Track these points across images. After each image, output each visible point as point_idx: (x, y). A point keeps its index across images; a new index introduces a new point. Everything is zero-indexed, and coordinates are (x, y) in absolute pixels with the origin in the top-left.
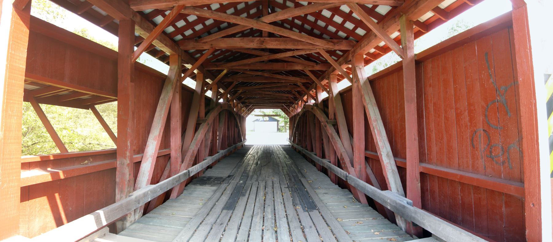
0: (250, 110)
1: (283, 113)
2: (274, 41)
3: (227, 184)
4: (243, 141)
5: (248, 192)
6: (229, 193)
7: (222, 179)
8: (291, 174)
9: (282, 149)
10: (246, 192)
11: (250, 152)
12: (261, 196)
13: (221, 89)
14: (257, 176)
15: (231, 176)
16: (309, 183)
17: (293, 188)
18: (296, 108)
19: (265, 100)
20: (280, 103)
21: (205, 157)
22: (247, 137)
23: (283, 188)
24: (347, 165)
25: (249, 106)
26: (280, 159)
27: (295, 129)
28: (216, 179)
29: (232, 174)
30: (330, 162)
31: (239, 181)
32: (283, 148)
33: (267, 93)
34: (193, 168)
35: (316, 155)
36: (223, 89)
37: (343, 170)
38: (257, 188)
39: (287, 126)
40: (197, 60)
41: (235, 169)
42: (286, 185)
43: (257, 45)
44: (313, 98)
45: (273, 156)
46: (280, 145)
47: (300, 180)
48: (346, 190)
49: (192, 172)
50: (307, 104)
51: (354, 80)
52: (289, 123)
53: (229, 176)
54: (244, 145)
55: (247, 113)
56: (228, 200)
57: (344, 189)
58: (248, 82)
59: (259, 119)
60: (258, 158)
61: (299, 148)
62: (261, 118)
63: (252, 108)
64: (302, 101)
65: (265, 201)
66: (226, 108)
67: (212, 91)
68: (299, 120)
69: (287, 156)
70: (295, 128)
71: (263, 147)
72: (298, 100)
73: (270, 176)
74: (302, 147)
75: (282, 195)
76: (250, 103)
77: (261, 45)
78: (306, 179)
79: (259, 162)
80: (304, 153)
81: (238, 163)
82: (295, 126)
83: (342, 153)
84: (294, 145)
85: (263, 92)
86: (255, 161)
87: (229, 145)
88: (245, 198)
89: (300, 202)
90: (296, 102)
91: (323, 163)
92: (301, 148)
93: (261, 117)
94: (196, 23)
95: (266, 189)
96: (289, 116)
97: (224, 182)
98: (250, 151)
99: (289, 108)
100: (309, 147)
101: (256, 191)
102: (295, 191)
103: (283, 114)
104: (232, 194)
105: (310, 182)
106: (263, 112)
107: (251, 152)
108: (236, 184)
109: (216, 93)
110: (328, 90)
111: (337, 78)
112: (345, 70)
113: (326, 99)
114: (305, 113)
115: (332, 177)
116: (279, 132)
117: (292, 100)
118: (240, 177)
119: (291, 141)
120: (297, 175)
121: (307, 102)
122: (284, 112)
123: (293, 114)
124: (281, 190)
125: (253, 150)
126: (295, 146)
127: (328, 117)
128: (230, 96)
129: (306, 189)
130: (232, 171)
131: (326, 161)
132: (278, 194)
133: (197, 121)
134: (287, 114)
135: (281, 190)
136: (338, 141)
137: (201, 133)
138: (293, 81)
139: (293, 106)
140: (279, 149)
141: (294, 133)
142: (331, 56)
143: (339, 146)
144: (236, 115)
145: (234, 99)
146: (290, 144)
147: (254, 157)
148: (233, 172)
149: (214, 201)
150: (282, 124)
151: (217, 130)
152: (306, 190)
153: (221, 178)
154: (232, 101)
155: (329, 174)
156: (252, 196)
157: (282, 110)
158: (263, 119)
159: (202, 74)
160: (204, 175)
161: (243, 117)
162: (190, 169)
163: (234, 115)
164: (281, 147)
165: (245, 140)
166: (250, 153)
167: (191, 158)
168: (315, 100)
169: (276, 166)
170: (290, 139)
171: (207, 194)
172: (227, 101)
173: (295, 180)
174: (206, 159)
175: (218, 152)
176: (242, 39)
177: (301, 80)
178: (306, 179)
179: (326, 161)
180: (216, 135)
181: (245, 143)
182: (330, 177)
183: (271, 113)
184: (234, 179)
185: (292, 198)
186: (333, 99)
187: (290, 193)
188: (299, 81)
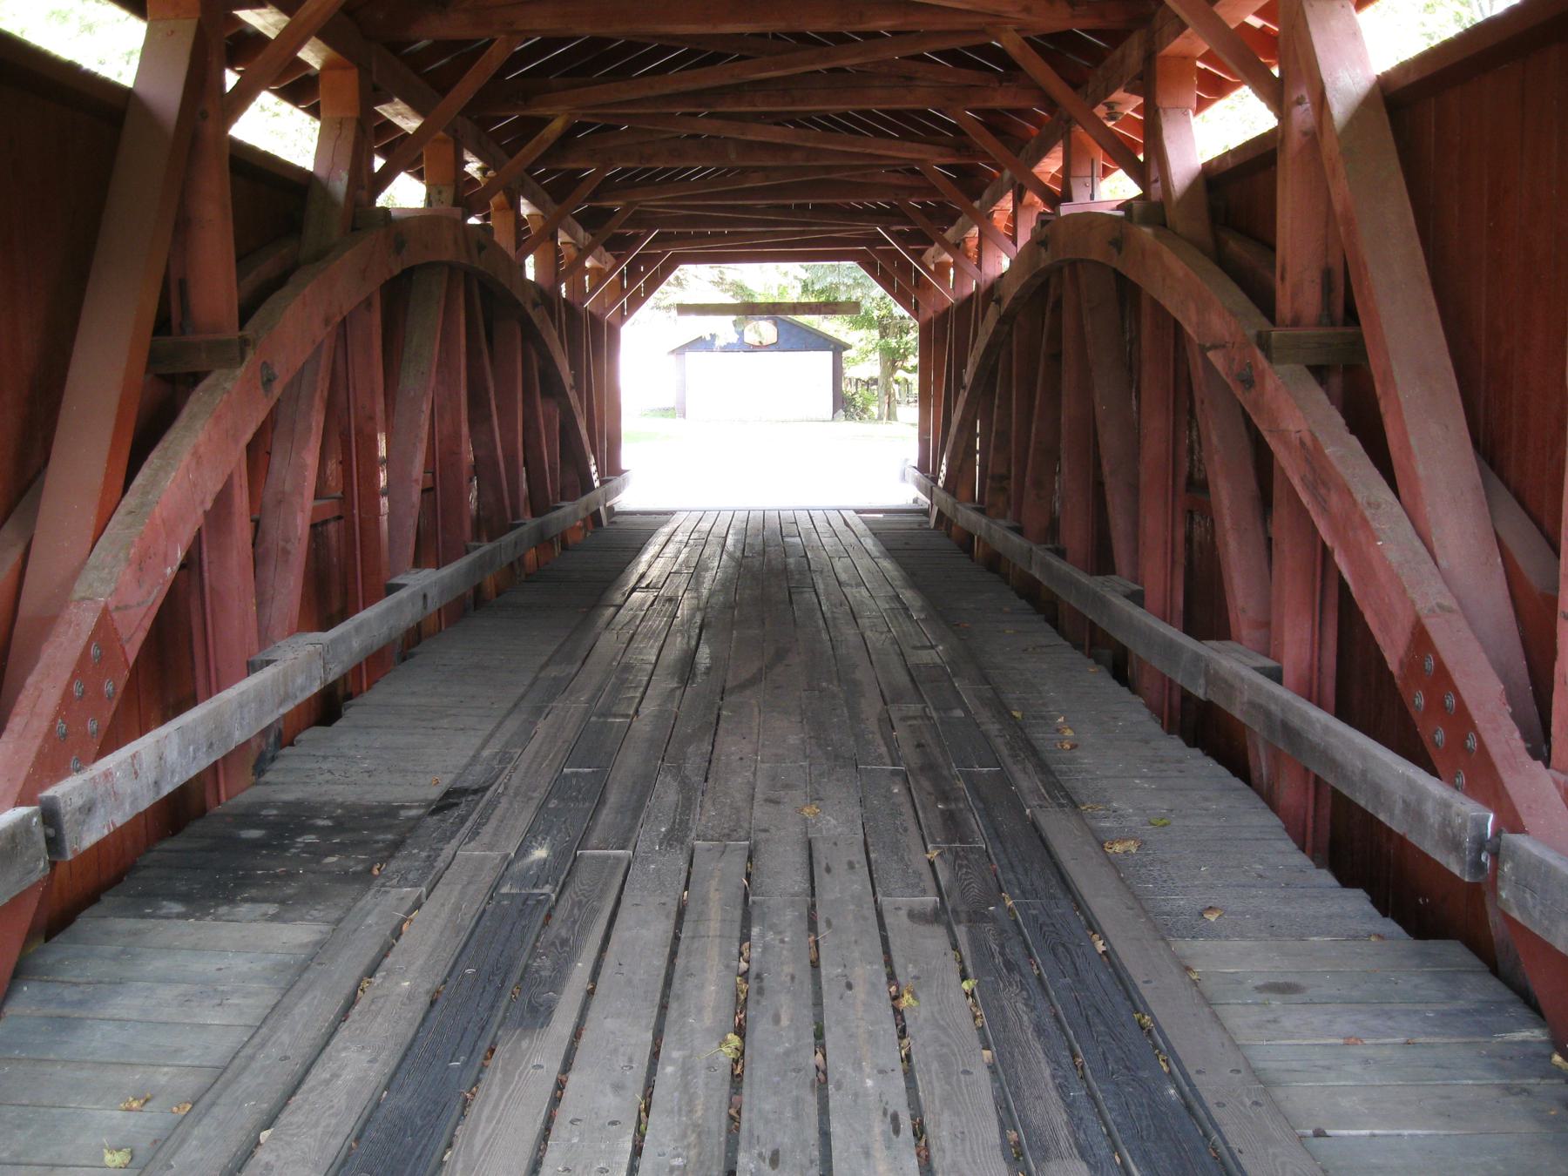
0: (647, 271)
1: (878, 291)
3: (415, 885)
4: (602, 483)
5: (581, 969)
6: (411, 996)
7: (388, 828)
8: (955, 770)
9: (869, 543)
10: (558, 980)
11: (642, 568)
12: (708, 1019)
13: (400, 106)
14: (685, 785)
15: (463, 792)
16: (1113, 863)
17: (988, 926)
18: (973, 253)
20: (853, 214)
21: (555, 501)
22: (628, 456)
23: (897, 922)
24: (1488, 738)
25: (636, 240)
26: (863, 622)
27: (967, 403)
28: (339, 826)
29: (470, 781)
30: (1276, 676)
31: (523, 851)
32: (877, 532)
33: (757, 134)
34: (107, 775)
35: (1137, 598)
36: (418, 108)
37: (1433, 772)
38: (672, 922)
39: (897, 382)
40: (443, 91)
41: (513, 724)
42: (924, 892)
44: (1121, 154)
45: (809, 596)
46: (858, 512)
47: (1035, 827)
48: (1454, 952)
49: (88, 809)
50: (1065, 210)
51: (1154, 174)
52: (913, 361)
53: (449, 800)
54: (610, 510)
55: (623, 291)
56: (387, 1087)
57: (1434, 946)
59: (713, 336)
60: (698, 619)
61: (995, 532)
62: (723, 326)
64: (1018, 200)
65: (736, 1080)
66: (447, 256)
67: (314, 111)
68: (995, 333)
69: (908, 595)
70: (963, 395)
71: (742, 515)
72: (986, 195)
73: (787, 786)
74: (1019, 531)
75: (898, 1012)
76: (642, 220)
78: (1080, 815)
79: (704, 656)
80: (1036, 573)
81: (543, 667)
82: (968, 378)
83: (1431, 625)
84: (956, 509)
85: (731, 131)
86: (678, 644)
87: (490, 524)
88: (544, 1052)
89: (1070, 1106)
90: (977, 204)
91: (1214, 679)
92: (1015, 538)
93: (730, 319)
95: (755, 931)
96: (915, 311)
97: (394, 865)
98: (646, 558)
99: (918, 255)
100: (1075, 534)
101: (660, 963)
102: (1010, 966)
103: (873, 294)
104: (433, 1003)
105: (1118, 848)
106: (739, 288)
107: (653, 563)
108: (487, 878)
109: (349, 134)
110: (1276, 71)
112: (1256, 22)
113: (1230, 163)
114: (1044, 286)
115: (1289, 791)
116: (849, 417)
118: (538, 795)
119: (935, 480)
120: (1004, 780)
121: (1067, 197)
122: (885, 281)
123: (951, 290)
124: (885, 942)
125: (671, 550)
126: (967, 517)
127: (1271, 317)
128: (483, 171)
129: (1104, 937)
130: (483, 747)
131: (1236, 666)
132: (860, 992)
133: (154, 358)
134: (902, 297)
135: (885, 942)
136: (1378, 506)
137: (186, 457)
138: (959, 23)
139: (950, 234)
140: (849, 538)
141: (953, 430)
143: (1393, 556)
144: (535, 305)
146: (925, 501)
147: (669, 607)
148: (486, 753)
149: (252, 1110)
150: (864, 366)
151: (372, 418)
152: (1100, 947)
153: (390, 811)
155: (1262, 764)
156: (610, 1024)
157: (870, 266)
158: (741, 334)
159: (356, 71)
160: (250, 795)
161: (596, 322)
162: (67, 790)
163: (518, 305)
164: (865, 521)
165: (616, 482)
166: (642, 576)
167: (77, 689)
168: (1139, 173)
169: (834, 688)
170: (922, 467)
171: (214, 1018)
172: (457, 202)
173: (996, 834)
174: (268, 663)
175: (392, 589)
178: (1080, 815)
179: (1236, 666)
180: (370, 463)
181: (616, 499)
182: (1269, 799)
183: (794, 296)
184: (488, 830)
185: (987, 1054)
186: (1330, 146)
187: (966, 986)
188: (935, 161)
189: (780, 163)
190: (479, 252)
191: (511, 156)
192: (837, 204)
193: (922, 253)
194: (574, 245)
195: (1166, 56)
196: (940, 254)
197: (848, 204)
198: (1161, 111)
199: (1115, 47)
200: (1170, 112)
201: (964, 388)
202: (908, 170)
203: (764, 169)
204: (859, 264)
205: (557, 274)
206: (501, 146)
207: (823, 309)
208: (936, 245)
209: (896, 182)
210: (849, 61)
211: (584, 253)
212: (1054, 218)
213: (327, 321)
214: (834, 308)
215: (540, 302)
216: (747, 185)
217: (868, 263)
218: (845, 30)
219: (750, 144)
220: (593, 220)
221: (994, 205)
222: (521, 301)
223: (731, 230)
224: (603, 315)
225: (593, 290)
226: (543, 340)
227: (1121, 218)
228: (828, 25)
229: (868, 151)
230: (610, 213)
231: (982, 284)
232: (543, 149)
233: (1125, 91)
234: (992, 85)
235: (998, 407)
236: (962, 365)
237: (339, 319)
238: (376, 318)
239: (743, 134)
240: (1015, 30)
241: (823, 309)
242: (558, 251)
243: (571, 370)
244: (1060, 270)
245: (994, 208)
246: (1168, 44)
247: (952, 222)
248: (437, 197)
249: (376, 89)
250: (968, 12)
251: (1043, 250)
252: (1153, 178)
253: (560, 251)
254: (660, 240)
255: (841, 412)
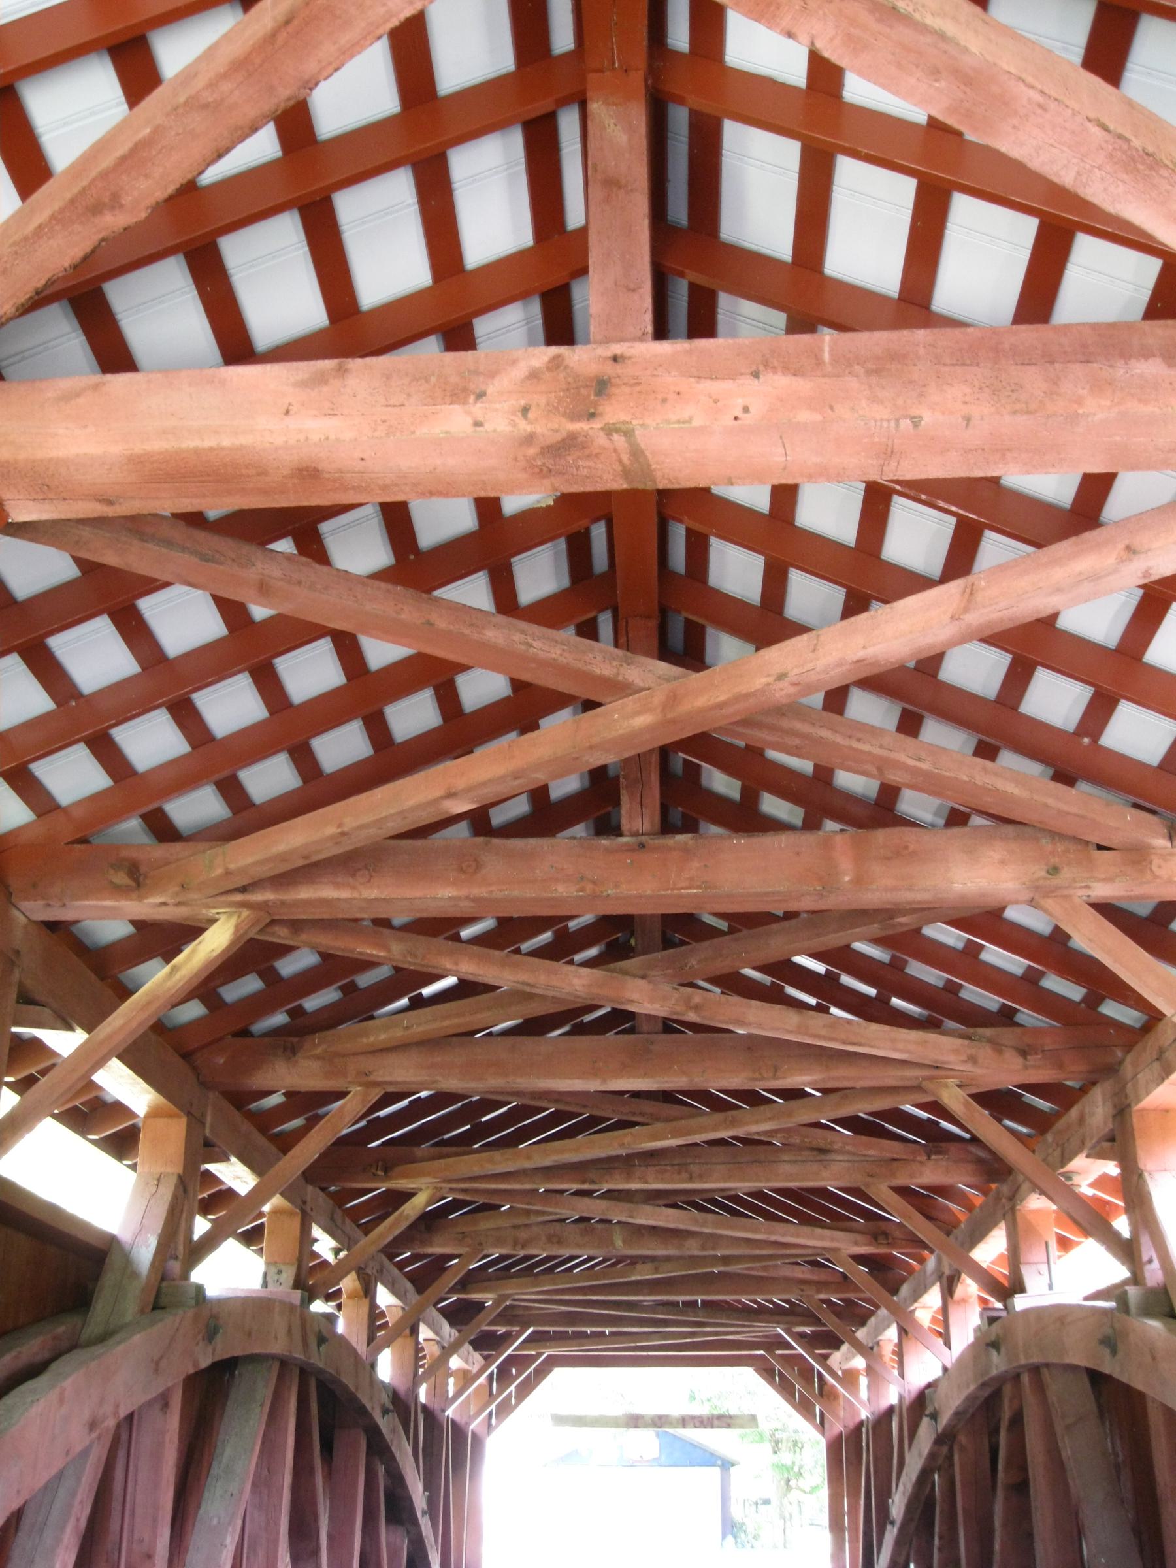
0: (519, 1374)
2: (733, 376)
19: (636, 1287)
20: (760, 1313)
25: (507, 1338)
27: (898, 1543)
40: (285, 1143)
43: (524, 427)
50: (1020, 1303)
51: (1147, 1251)
58: (555, 1257)
63: (531, 1359)
64: (949, 1291)
66: (277, 1347)
67: (260, 1252)
72: (905, 1290)
76: (512, 1315)
77: (574, 417)
82: (897, 1506)
85: (618, 1213)
94: (310, 981)
109: (167, 1192)
111: (1057, 1234)
117: (831, 1323)
121: (1018, 1286)
134: (804, 1408)
139: (861, 1334)
142: (999, 1121)
144: (385, 1412)
145: (381, 1276)
154: (408, 1331)
157: (767, 1373)
159: (184, 1120)
163: (363, 1411)
172: (298, 1284)
176: (320, 379)
177: (973, 1059)
189: (671, 1252)
190: (319, 1346)
191: (366, 1234)
192: (726, 1302)
193: (826, 1357)
194: (438, 1342)
195: (1143, 1110)
196: (848, 1359)
197: (740, 1302)
198: (1146, 1175)
199: (1068, 1106)
200: (1157, 1176)
201: (892, 1523)
202: (809, 1262)
203: (653, 1259)
204: (755, 1370)
205: (415, 1374)
206: (359, 1226)
207: (716, 1422)
208: (845, 1347)
209: (800, 1276)
210: (756, 1125)
211: (448, 1351)
212: (1004, 1314)
213: (92, 1425)
214: (729, 1421)
215: (391, 1407)
216: (633, 1278)
217: (765, 1370)
218: (758, 1087)
219: (641, 1227)
220: (459, 1315)
221: (915, 1301)
222: (368, 1407)
223: (614, 1329)
224: (468, 1424)
225: (458, 1394)
226: (392, 1453)
227: (1111, 1310)
228: (737, 1081)
229: (773, 1238)
230: (480, 1306)
231: (906, 1395)
232: (404, 1225)
233: (1088, 1157)
234: (918, 1158)
235: (940, 1549)
236: (884, 1494)
237: (111, 1423)
238: (172, 1424)
239: (631, 1217)
240: (959, 1086)
241: (716, 1422)
242: (418, 1349)
243: (425, 1490)
244: (1017, 1377)
245: (916, 1305)
246: (1148, 1093)
247: (863, 1322)
248: (276, 1277)
249: (207, 1144)
250: (903, 1063)
251: (994, 1353)
252: (1145, 1258)
253: (422, 1349)
254: (538, 1339)
255: (730, 1538)
